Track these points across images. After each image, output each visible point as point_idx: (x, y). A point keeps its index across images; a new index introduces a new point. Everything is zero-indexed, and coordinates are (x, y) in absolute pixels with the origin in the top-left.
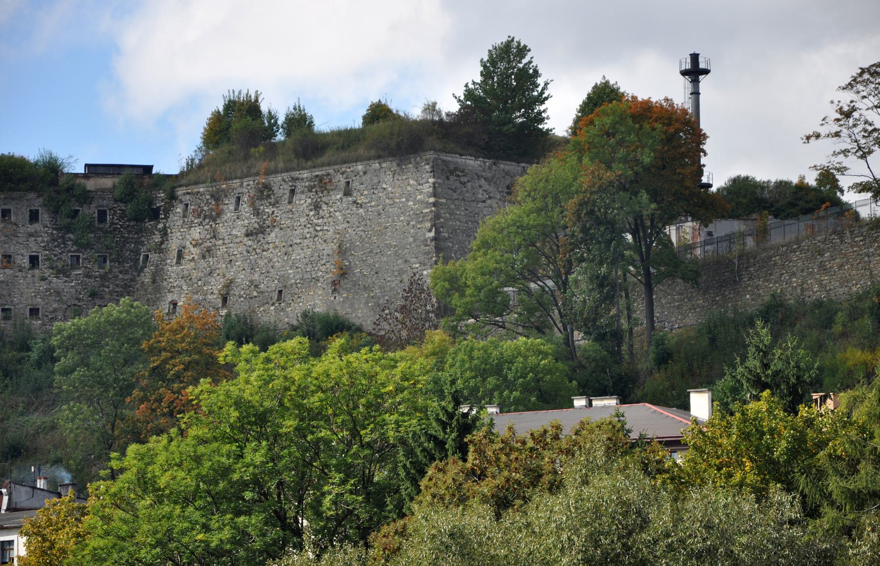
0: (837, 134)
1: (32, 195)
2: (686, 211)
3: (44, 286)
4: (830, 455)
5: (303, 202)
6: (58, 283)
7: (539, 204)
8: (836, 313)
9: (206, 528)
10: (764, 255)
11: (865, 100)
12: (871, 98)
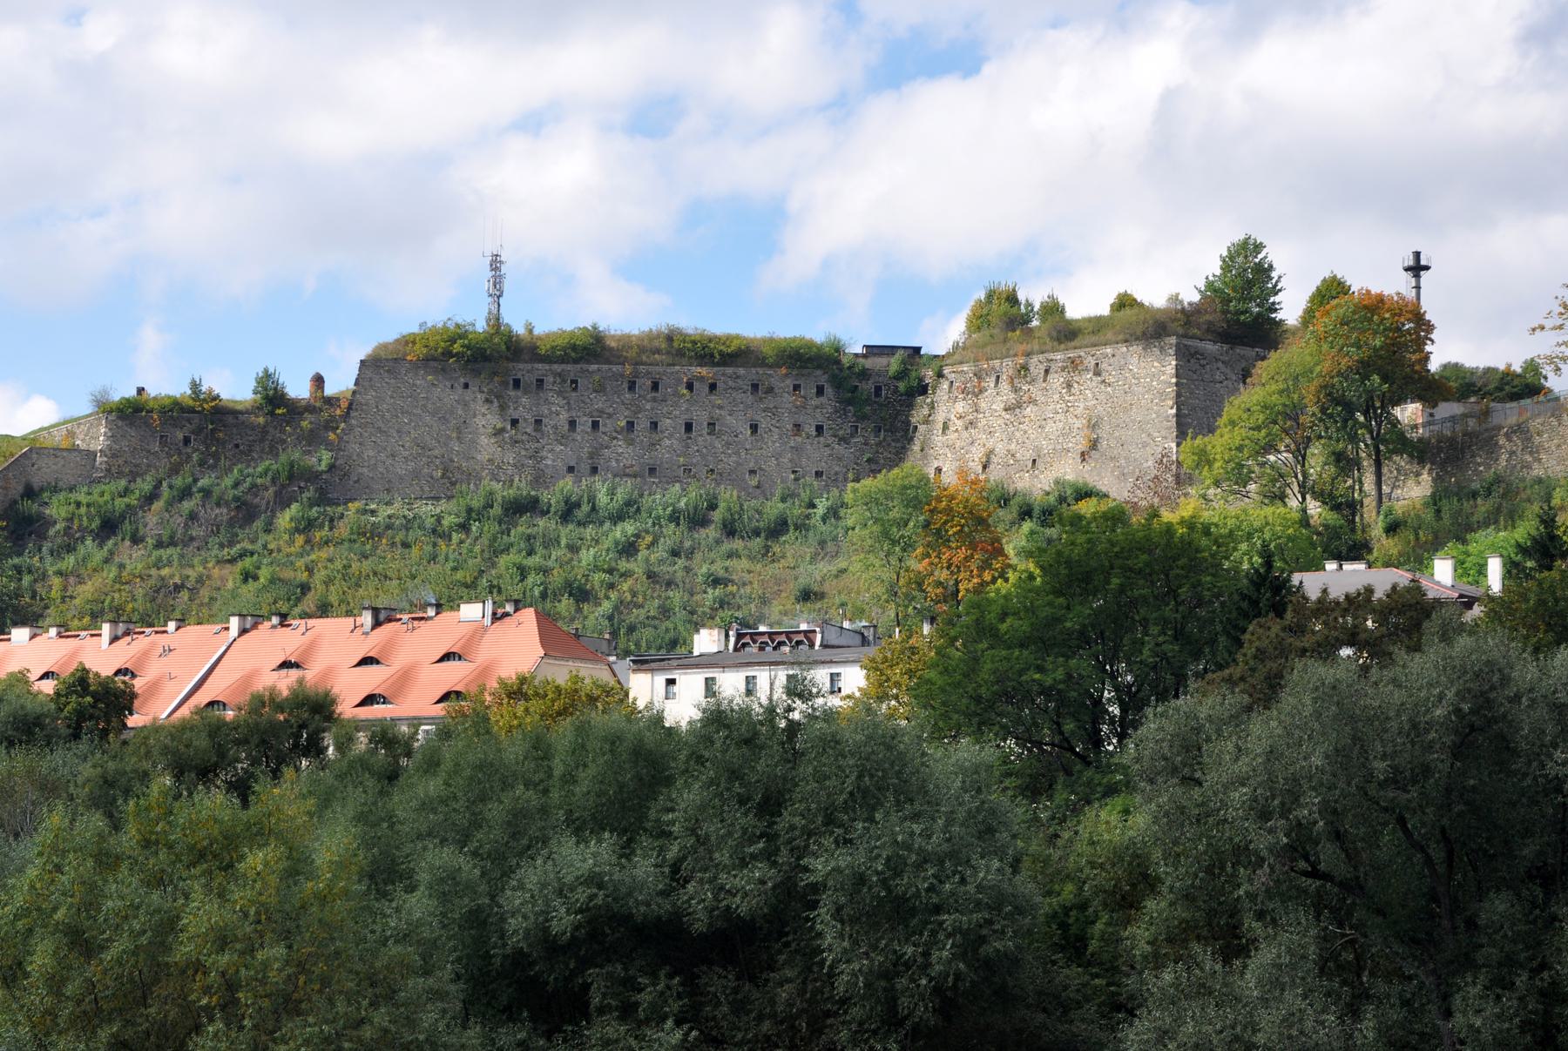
1: (819, 372)
3: (828, 451)
5: (1057, 380)
6: (840, 449)
7: (1282, 386)
9: (1040, 669)
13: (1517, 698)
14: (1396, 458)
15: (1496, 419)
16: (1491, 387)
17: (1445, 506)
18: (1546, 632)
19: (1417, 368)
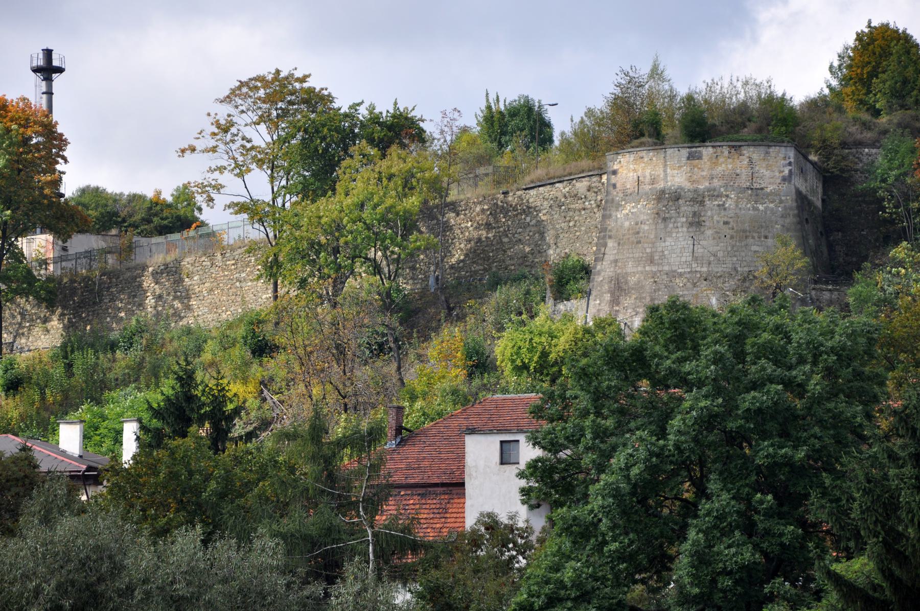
0: (214, 149)
2: (42, 223)
4: (260, 497)
8: (205, 341)
10: (129, 274)
11: (244, 115)
12: (250, 113)
13: (130, 590)
14: (21, 301)
15: (139, 258)
16: (137, 217)
17: (78, 359)
18: (177, 511)
19: (47, 191)
